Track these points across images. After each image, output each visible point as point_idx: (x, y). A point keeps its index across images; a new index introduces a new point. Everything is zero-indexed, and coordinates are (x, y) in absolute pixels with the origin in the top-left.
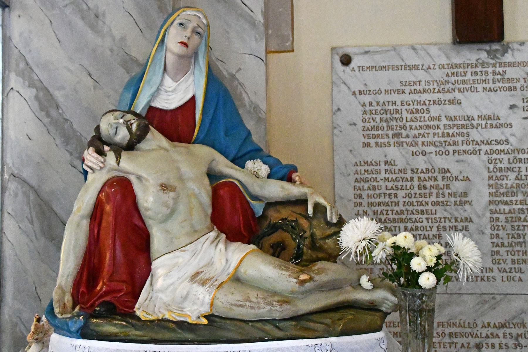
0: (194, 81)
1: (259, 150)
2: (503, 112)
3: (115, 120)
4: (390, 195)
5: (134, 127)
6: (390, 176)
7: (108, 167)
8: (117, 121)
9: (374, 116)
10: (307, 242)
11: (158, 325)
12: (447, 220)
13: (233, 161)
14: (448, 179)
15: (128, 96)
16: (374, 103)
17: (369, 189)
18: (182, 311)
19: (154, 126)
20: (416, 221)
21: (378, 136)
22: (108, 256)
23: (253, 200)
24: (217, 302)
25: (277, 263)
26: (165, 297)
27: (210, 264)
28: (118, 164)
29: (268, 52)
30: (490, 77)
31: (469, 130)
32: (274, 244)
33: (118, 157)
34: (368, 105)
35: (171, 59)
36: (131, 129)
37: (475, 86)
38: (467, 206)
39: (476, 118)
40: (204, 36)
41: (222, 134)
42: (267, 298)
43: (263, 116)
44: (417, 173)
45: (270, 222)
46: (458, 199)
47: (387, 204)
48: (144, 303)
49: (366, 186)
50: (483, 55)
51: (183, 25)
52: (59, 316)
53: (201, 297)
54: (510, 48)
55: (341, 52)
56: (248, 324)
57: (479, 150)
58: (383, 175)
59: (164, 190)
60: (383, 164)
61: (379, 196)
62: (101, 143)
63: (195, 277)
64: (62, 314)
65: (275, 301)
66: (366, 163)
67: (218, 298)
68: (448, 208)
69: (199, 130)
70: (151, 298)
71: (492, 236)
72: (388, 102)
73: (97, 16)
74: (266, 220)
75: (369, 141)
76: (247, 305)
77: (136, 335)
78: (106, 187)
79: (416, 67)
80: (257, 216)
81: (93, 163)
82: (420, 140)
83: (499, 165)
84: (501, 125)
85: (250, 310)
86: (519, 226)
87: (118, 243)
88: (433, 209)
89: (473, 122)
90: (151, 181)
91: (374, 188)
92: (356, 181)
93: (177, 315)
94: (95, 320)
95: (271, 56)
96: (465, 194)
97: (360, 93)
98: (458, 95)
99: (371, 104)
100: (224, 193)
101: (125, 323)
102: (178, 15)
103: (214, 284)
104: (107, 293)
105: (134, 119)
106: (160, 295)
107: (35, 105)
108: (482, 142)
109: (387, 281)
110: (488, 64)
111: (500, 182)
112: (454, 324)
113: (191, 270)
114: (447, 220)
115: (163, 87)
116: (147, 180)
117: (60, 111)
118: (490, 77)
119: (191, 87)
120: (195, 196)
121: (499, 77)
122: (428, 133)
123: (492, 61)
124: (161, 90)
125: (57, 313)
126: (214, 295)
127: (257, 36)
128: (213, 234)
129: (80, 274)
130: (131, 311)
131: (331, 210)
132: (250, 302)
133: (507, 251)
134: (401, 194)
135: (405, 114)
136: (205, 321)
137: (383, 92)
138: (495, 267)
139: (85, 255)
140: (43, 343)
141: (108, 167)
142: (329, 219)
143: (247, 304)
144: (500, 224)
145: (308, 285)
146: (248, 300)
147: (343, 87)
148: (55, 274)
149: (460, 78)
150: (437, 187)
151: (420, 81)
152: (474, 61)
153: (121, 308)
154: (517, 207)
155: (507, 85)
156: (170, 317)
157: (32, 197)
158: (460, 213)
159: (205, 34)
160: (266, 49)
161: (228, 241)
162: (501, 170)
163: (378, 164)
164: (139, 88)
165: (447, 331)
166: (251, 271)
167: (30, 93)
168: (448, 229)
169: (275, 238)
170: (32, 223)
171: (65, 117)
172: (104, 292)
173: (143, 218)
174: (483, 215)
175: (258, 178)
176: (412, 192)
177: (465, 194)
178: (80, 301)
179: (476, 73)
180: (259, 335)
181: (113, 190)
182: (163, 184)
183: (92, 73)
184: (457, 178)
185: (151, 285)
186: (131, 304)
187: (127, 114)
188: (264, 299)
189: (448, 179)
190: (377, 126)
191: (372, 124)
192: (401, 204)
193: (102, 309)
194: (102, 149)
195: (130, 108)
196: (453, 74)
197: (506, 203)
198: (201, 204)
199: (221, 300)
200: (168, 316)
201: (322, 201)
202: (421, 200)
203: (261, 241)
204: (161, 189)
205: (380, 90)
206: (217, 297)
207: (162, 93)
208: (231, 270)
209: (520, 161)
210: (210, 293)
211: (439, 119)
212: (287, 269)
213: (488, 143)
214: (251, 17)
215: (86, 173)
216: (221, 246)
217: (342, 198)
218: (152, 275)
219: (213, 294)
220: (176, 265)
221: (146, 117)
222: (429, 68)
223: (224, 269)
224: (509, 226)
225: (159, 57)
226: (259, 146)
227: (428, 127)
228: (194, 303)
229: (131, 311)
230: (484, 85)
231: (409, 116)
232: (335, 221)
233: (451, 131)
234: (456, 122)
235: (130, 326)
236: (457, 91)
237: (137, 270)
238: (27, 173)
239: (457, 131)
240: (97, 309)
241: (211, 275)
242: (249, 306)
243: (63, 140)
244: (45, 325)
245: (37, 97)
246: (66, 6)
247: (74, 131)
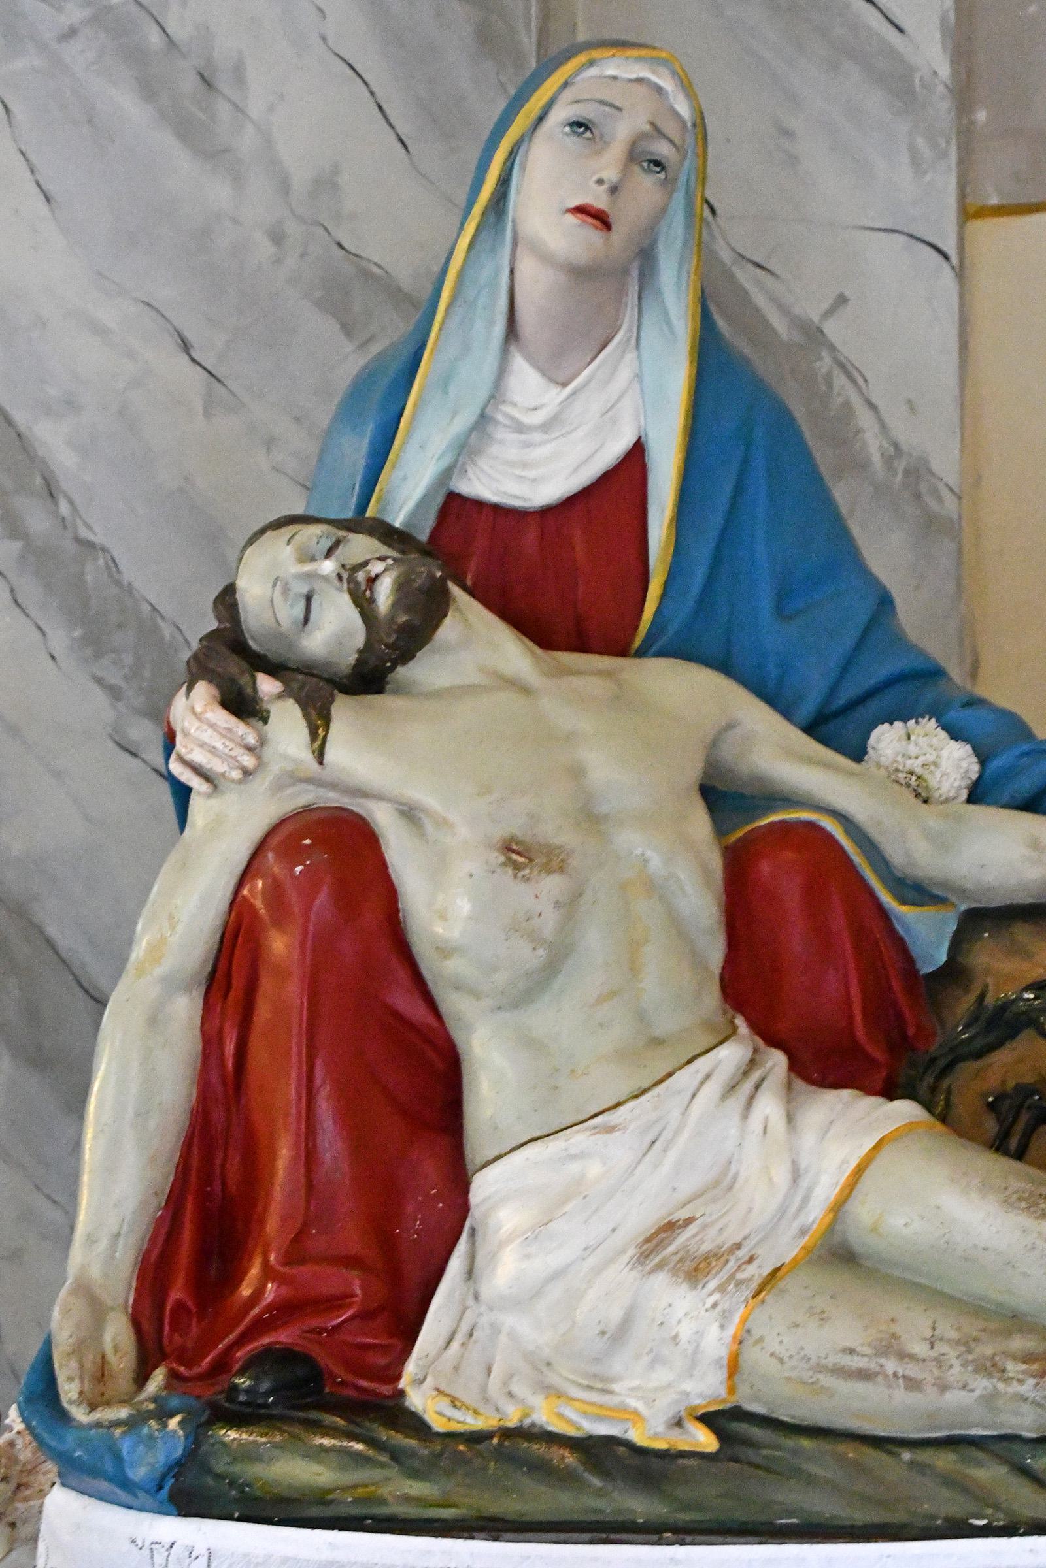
0: (639, 377)
1: (934, 673)
3: (301, 561)
5: (384, 595)
7: (275, 768)
8: (308, 567)
11: (500, 1455)
13: (811, 729)
18: (605, 1391)
19: (469, 583)
22: (284, 1154)
23: (904, 902)
24: (753, 1356)
25: (1015, 1184)
28: (320, 756)
29: (969, 212)
32: (1000, 1097)
36: (372, 600)
40: (682, 180)
41: (765, 599)
42: (976, 1340)
43: (950, 505)
45: (982, 996)
48: (439, 1354)
51: (587, 128)
52: (80, 1414)
53: (686, 1331)
56: (897, 1455)
59: (517, 867)
62: (245, 665)
64: (93, 1407)
65: (1014, 1358)
67: (761, 1339)
69: (663, 596)
70: (471, 1335)
73: (207, 82)
74: (967, 989)
76: (890, 1371)
77: (407, 1499)
78: (271, 856)
80: (926, 969)
81: (213, 750)
85: (901, 1397)
90: (463, 831)
93: (585, 1414)
94: (233, 1434)
95: (981, 228)
101: (359, 1447)
102: (566, 85)
103: (740, 1276)
104: (284, 1311)
105: (382, 559)
106: (509, 1320)
115: (503, 408)
116: (443, 823)
117: (64, 508)
119: (627, 407)
120: (652, 887)
124: (497, 422)
125: (71, 1402)
126: (744, 1321)
127: (921, 142)
128: (731, 1055)
129: (164, 1230)
130: (386, 1389)
132: (903, 1356)
139: (187, 1146)
140: (13, 1525)
141: (275, 768)
146: (890, 1346)
148: (56, 1215)
153: (342, 1375)
156: (555, 1420)
159: (687, 163)
160: (962, 196)
161: (799, 1084)
164: (401, 415)
166: (902, 1221)
171: (84, 533)
172: (269, 1308)
173: (430, 984)
175: (926, 801)
178: (168, 1350)
180: (949, 1505)
181: (299, 869)
182: (512, 839)
183: (190, 336)
185: (470, 1273)
186: (382, 1361)
187: (352, 536)
188: (966, 1344)
193: (265, 1386)
194: (249, 690)
198: (676, 924)
199: (772, 1344)
200: (545, 1416)
203: (945, 1084)
204: (504, 864)
206: (757, 1333)
207: (500, 434)
208: (815, 1213)
210: (725, 1317)
214: (892, 53)
215: (182, 793)
216: (769, 1106)
218: (473, 1232)
219: (737, 1319)
221: (433, 548)
223: (782, 1212)
225: (486, 274)
226: (927, 657)
228: (657, 1360)
229: (386, 1389)
235: (384, 1458)
237: (410, 1209)
240: (243, 1382)
241: (732, 1236)
242: (895, 1374)
243: (78, 633)
244: (20, 1443)
246: (71, 33)
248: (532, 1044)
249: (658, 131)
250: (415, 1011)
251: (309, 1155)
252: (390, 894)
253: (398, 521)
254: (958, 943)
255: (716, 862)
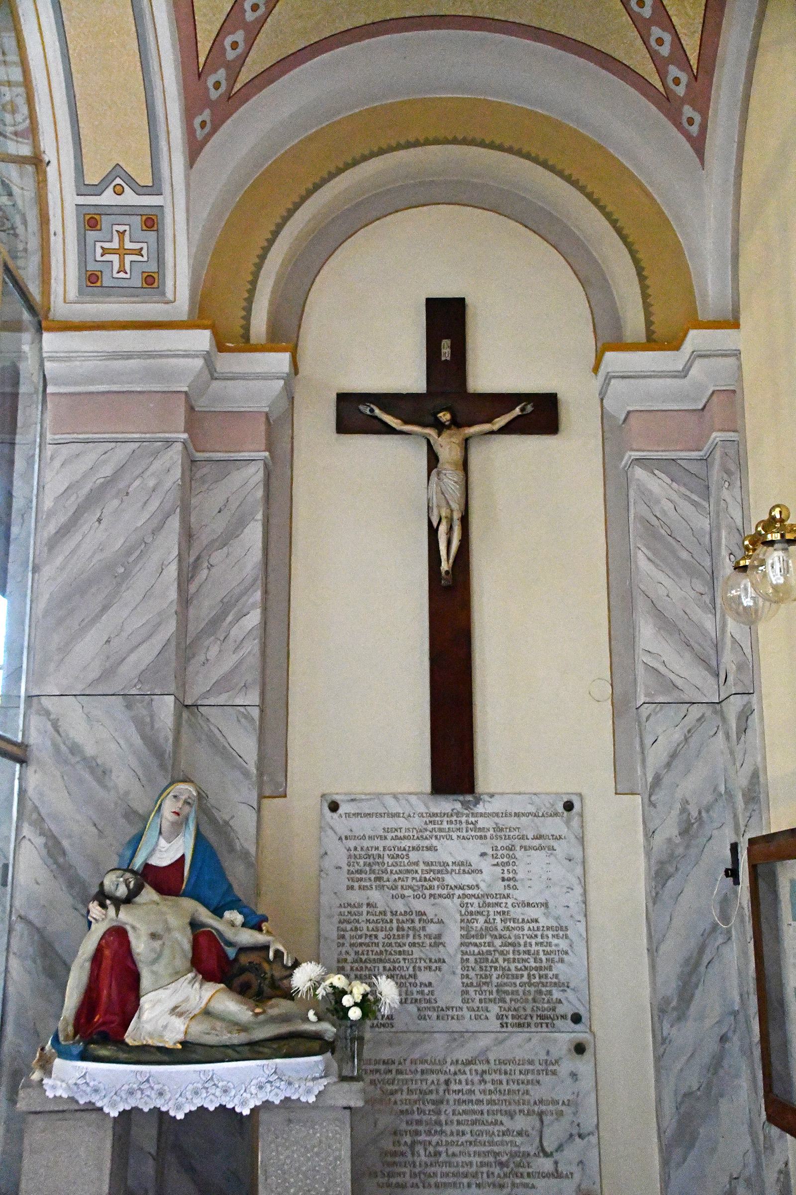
2: (475, 859)
4: (371, 936)
6: (371, 918)
9: (358, 861)
10: (267, 982)
12: (422, 962)
14: (424, 921)
15: (128, 854)
16: (359, 849)
17: (351, 930)
20: (394, 962)
21: (361, 879)
26: (148, 1027)
27: (187, 1000)
28: (117, 915)
29: (261, 797)
30: (464, 825)
31: (444, 876)
33: (117, 910)
34: (352, 849)
35: (166, 825)
37: (451, 834)
38: (441, 947)
39: (450, 864)
44: (396, 915)
46: (433, 941)
47: (367, 945)
49: (349, 927)
50: (458, 806)
52: (63, 1043)
54: (481, 799)
55: (329, 799)
57: (453, 895)
58: (364, 917)
60: (365, 907)
61: (361, 937)
63: (175, 1011)
66: (349, 905)
68: (422, 949)
71: (462, 976)
72: (372, 847)
75: (352, 884)
79: (397, 815)
82: (400, 883)
83: (470, 909)
84: (473, 871)
86: (486, 967)
87: (113, 984)
88: (410, 949)
89: (447, 867)
91: (356, 929)
92: (340, 922)
95: (266, 802)
96: (439, 936)
97: (346, 838)
98: (434, 842)
99: (356, 849)
100: (203, 941)
107: (44, 852)
108: (456, 887)
109: (329, 1015)
110: (463, 814)
111: (470, 925)
112: (426, 1061)
113: (172, 1005)
114: (422, 962)
116: (139, 929)
118: (464, 825)
121: (471, 826)
122: (407, 878)
123: (466, 812)
131: (287, 955)
133: (476, 991)
134: (381, 935)
135: (386, 859)
136: (179, 1046)
137: (367, 838)
138: (465, 1006)
141: (109, 918)
142: (285, 962)
143: (213, 1032)
144: (470, 965)
145: (261, 1017)
146: (214, 1029)
147: (330, 832)
149: (437, 826)
150: (414, 929)
151: (400, 829)
152: (449, 811)
154: (484, 949)
155: (479, 834)
157: (36, 938)
158: (434, 954)
162: (471, 913)
163: (360, 905)
165: (420, 1067)
167: (40, 841)
168: (423, 969)
169: (244, 977)
170: (35, 962)
174: (455, 955)
176: (391, 933)
177: (439, 936)
179: (451, 822)
180: (220, 1057)
184: (432, 921)
185: (139, 1017)
189: (424, 921)
190: (361, 870)
191: (357, 867)
192: (380, 945)
195: (129, 865)
196: (431, 822)
197: (476, 945)
200: (150, 1042)
201: (281, 948)
202: (399, 941)
205: (364, 835)
208: (203, 1005)
209: (489, 905)
211: (417, 864)
212: (245, 1004)
213: (461, 888)
214: (246, 769)
215: (90, 923)
216: (197, 985)
217: (326, 939)
220: (159, 1001)
222: (409, 816)
224: (477, 968)
227: (408, 871)
228: (172, 1032)
230: (459, 834)
231: (391, 861)
232: (290, 965)
233: (428, 876)
234: (432, 868)
236: (434, 838)
238: (32, 915)
239: (433, 876)
245: (46, 844)
246: (78, 762)
247: (78, 875)
248: (154, 973)
249: (189, 798)
250: (130, 964)
251: (109, 995)
252: (129, 942)
253: (135, 869)
254: (237, 954)
255: (191, 937)
